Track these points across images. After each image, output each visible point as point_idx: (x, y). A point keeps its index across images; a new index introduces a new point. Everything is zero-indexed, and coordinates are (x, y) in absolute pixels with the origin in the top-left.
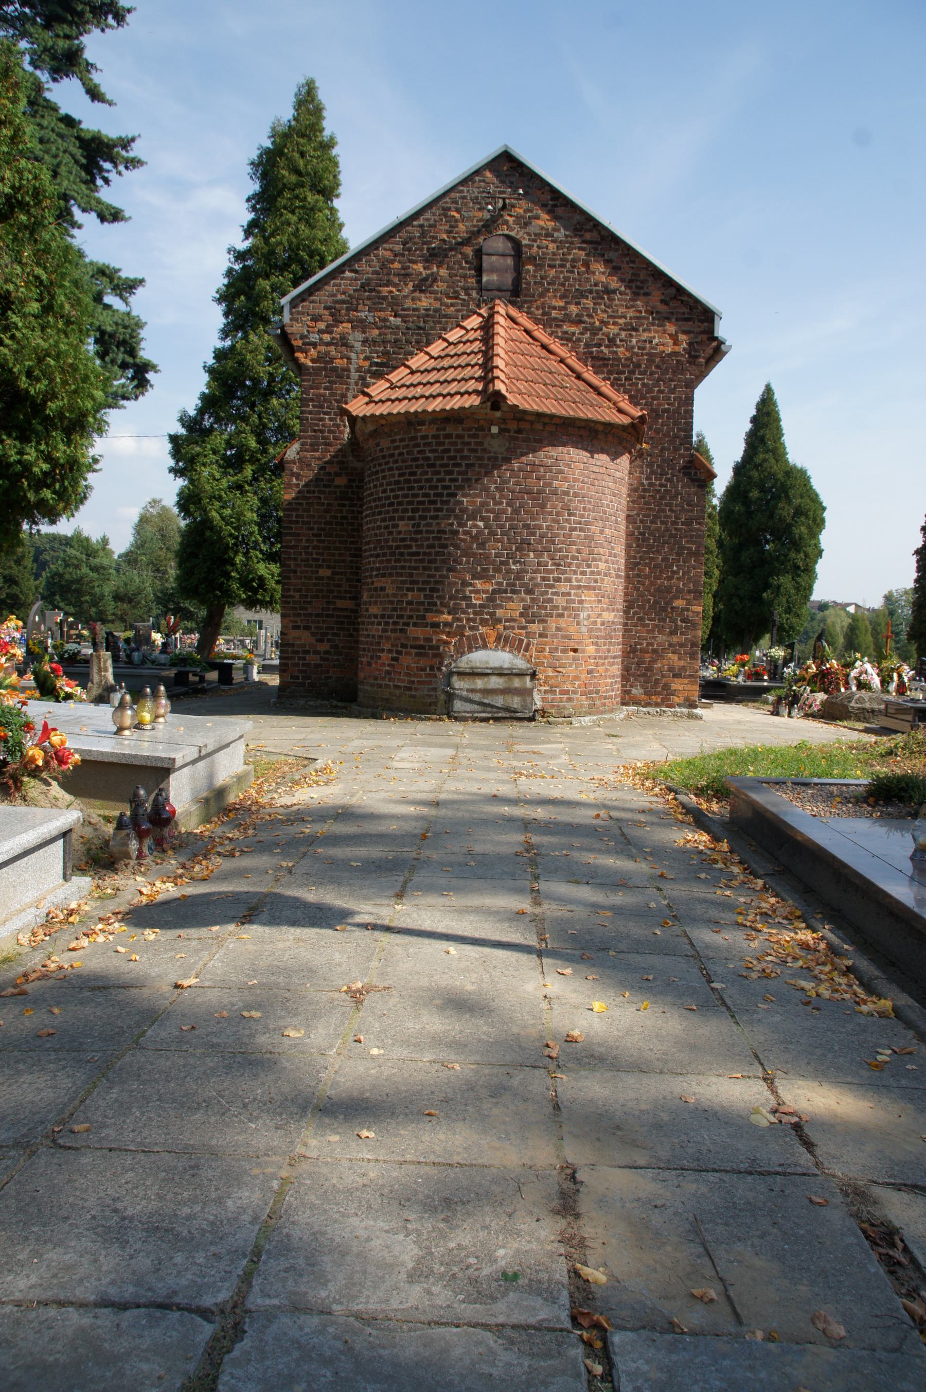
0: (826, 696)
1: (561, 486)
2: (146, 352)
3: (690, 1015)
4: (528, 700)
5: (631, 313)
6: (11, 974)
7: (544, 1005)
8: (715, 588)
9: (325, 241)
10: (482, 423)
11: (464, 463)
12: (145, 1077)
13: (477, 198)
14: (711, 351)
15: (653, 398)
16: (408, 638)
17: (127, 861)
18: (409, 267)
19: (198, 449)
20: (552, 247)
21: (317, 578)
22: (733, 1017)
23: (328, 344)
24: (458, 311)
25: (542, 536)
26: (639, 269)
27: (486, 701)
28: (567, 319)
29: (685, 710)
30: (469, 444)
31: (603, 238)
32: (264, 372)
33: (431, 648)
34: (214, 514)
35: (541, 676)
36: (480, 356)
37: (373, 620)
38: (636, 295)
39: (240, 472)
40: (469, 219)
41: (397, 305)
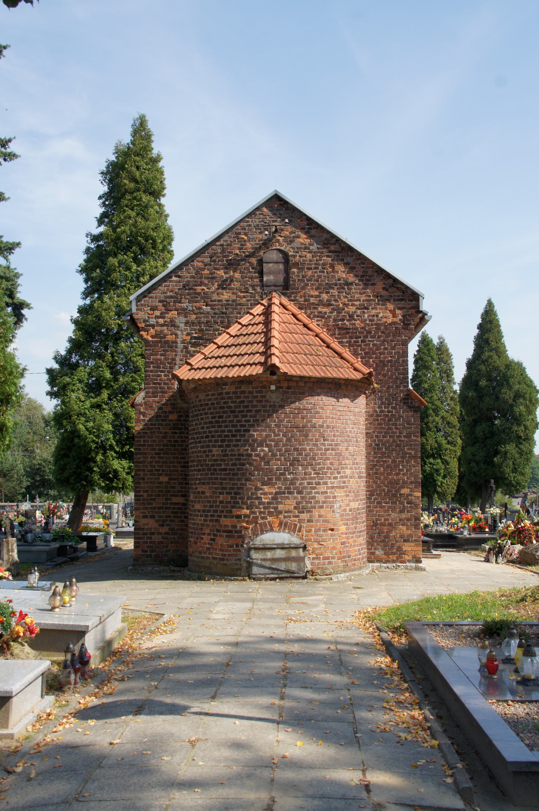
0: (522, 547)
1: (318, 421)
2: (22, 295)
3: (341, 747)
4: (302, 564)
5: (363, 298)
6: (32, 744)
7: (276, 744)
8: (459, 454)
9: (155, 229)
10: (264, 383)
11: (254, 410)
12: (107, 777)
13: (258, 225)
14: (418, 320)
16: (221, 526)
17: (69, 686)
18: (215, 273)
19: (68, 379)
20: (309, 256)
21: (158, 483)
22: (359, 747)
23: (162, 325)
24: (248, 301)
26: (367, 268)
27: (274, 566)
28: (321, 303)
29: (413, 565)
30: (257, 397)
31: (342, 249)
32: (115, 324)
34: (81, 426)
35: (310, 548)
36: (262, 335)
37: (197, 513)
38: (366, 285)
39: (99, 395)
40: (254, 239)
41: (207, 298)
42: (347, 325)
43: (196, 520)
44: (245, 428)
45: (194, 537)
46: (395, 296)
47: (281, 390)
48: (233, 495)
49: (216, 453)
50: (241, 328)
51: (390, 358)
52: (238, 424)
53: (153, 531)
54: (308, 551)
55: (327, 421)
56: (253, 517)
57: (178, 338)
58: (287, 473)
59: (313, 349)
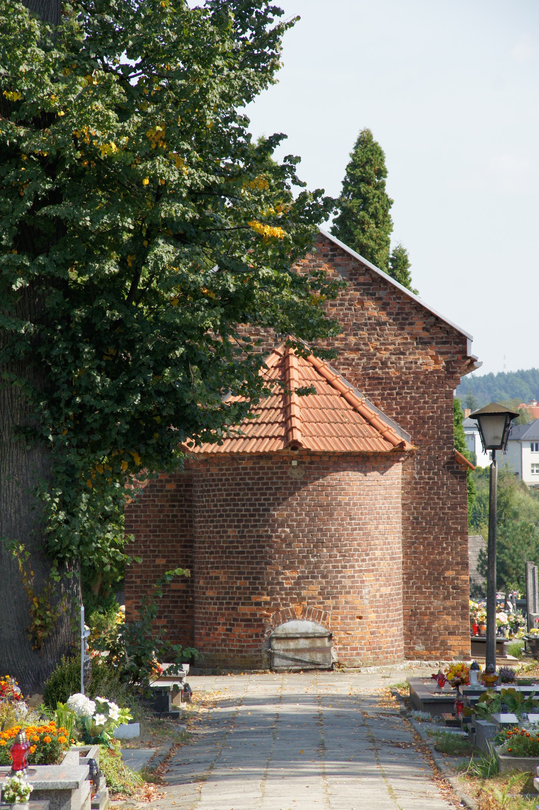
1: (344, 499)
4: (328, 655)
5: (399, 340)
10: (285, 458)
11: (273, 487)
15: (420, 408)
16: (238, 614)
21: (153, 566)
25: (331, 536)
26: (404, 303)
27: (297, 657)
30: (277, 473)
31: (374, 280)
33: (256, 620)
35: (336, 638)
37: (210, 601)
42: (379, 375)
43: (208, 609)
46: (437, 337)
48: (252, 580)
51: (431, 414)
52: (257, 502)
54: (334, 640)
56: (274, 604)
58: (310, 555)
59: (338, 415)
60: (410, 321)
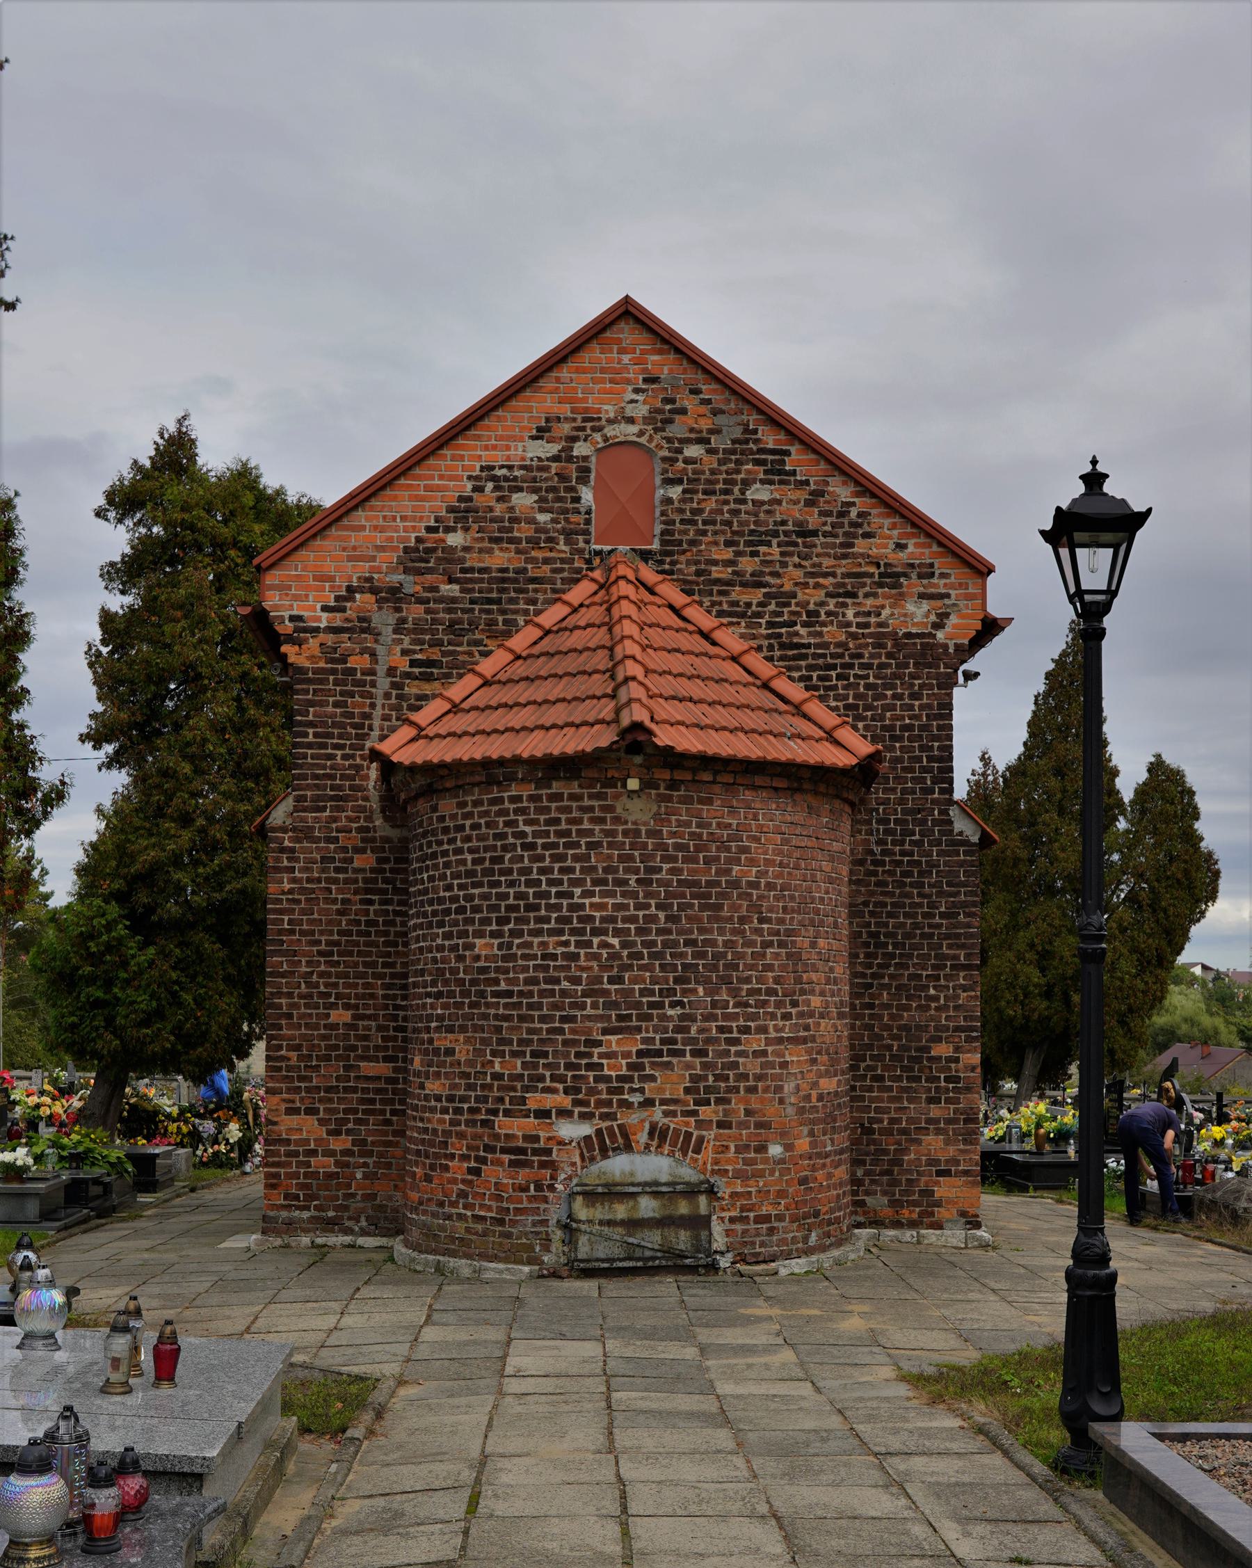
1: (746, 874)
4: (704, 1234)
16: (497, 1137)
21: (325, 1026)
24: (554, 571)
30: (591, 809)
33: (536, 1152)
37: (433, 1103)
43: (429, 1121)
44: (560, 889)
45: (424, 1164)
47: (653, 792)
48: (528, 1058)
49: (484, 953)
50: (541, 638)
53: (312, 1146)
55: (767, 872)
57: (377, 662)
60: (866, 528)
